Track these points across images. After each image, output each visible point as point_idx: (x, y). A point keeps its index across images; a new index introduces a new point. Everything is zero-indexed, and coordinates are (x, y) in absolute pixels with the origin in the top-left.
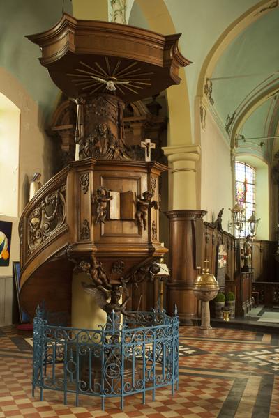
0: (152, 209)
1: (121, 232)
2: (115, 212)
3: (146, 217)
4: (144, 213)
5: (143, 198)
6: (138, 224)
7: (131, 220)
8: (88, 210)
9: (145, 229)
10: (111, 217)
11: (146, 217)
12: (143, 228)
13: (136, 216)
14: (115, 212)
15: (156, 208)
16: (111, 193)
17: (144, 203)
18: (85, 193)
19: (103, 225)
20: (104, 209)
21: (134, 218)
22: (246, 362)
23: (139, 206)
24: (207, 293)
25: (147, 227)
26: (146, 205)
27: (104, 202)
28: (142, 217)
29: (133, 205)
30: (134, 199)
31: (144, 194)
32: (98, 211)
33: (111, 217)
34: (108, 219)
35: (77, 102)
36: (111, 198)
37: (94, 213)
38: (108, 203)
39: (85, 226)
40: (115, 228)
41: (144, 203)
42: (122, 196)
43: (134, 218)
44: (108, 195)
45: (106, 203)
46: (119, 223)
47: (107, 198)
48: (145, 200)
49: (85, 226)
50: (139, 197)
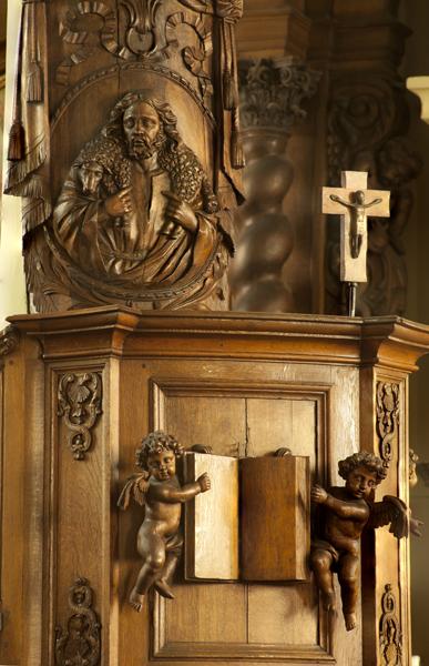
2: (214, 549)
5: (339, 482)
6: (318, 600)
7: (286, 583)
9: (349, 626)
13: (311, 564)
14: (214, 549)
15: (398, 531)
18: (83, 458)
19: (161, 606)
20: (167, 535)
21: (300, 574)
23: (322, 521)
27: (171, 501)
28: (339, 567)
30: (301, 485)
31: (347, 467)
33: (201, 571)
34: (184, 574)
38: (188, 508)
39: (80, 609)
40: (212, 620)
46: (233, 595)
48: (347, 494)
49: (80, 609)
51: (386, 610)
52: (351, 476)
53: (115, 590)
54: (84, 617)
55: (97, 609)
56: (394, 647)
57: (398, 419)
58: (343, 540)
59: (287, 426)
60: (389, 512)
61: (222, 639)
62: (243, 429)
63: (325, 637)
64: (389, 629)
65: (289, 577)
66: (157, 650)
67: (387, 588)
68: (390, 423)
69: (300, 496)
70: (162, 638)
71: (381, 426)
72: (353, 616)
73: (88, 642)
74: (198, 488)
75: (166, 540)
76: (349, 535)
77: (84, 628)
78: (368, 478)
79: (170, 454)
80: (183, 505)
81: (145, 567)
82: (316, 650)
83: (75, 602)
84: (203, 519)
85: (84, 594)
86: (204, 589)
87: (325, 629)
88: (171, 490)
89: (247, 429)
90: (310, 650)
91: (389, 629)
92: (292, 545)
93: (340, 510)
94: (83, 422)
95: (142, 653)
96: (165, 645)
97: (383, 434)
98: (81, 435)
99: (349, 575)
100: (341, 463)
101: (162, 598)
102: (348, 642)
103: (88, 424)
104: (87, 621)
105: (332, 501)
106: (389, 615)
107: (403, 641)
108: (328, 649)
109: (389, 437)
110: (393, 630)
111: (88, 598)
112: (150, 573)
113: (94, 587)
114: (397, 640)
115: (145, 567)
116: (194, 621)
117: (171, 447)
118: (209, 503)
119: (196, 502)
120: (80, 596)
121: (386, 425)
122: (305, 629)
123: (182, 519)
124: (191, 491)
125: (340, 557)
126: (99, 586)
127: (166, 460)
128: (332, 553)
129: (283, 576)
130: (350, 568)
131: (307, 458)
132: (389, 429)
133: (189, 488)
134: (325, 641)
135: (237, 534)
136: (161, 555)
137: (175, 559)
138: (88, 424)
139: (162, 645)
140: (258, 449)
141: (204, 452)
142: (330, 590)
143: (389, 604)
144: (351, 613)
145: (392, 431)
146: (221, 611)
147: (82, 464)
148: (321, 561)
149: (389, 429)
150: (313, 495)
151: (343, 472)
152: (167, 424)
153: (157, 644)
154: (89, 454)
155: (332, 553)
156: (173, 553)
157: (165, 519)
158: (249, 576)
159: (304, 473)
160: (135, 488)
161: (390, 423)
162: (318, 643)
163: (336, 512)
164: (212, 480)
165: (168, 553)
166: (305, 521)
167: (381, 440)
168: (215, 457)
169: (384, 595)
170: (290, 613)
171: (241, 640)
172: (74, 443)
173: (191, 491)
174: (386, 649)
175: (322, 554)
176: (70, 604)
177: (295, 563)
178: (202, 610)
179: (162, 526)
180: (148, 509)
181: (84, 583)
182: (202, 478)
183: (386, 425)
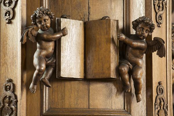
0: (155, 55)
1: (85, 106)
2: (71, 64)
3: (141, 74)
4: (136, 65)
5: (133, 32)
6: (123, 88)
7: (107, 80)
8: (13, 63)
9: (138, 100)
10: (65, 73)
11: (141, 74)
12: (135, 98)
13: (118, 71)
14: (71, 64)
15: (162, 54)
16: (65, 23)
17: (136, 44)
18: (10, 22)
19: (46, 91)
20: (47, 57)
21: (113, 75)
22: (168, 17)
23: (123, 50)
24: (47, 21)
25: (143, 95)
26: (139, 48)
27: (49, 40)
28: (131, 72)
29: (112, 48)
30: (114, 34)
31: (136, 24)
32: (36, 61)
33: (65, 73)
34: (56, 77)
35: (145, 39)
36: (64, 32)
37: (27, 65)
38: (58, 44)
39: (9, 93)
40: (73, 99)
41: (136, 44)
42: (88, 29)
43: (113, 75)
44: (56, 27)
45: (51, 45)
46: (82, 86)
47: (55, 32)
48: (137, 38)
49: (9, 93)
50: (125, 31)
51: (159, 93)
52: (138, 28)
53: (24, 84)
54: (10, 97)
55: (16, 93)
56: (163, 111)
57: (166, 4)
58: (134, 59)
59: (109, 7)
60: (157, 46)
61: (76, 107)
62: (87, 8)
63: (127, 106)
64: (160, 102)
65: (107, 76)
66: (44, 112)
67: (160, 83)
68: (161, 6)
69: (113, 39)
70: (47, 106)
71: (157, 8)
72: (140, 95)
73: (12, 109)
74: (62, 34)
75: (47, 59)
76: (137, 57)
77: (10, 102)
78: (146, 28)
79: (47, 17)
80: (55, 42)
81: (36, 72)
82: (123, 112)
83: (6, 89)
84: (65, 49)
85: (10, 86)
86: (68, 84)
87: (128, 102)
88: (47, 35)
89: (89, 8)
90: (120, 112)
91: (160, 102)
92: (109, 62)
93: (132, 44)
94: (10, 5)
95: (38, 114)
96: (49, 109)
97: (157, 11)
98: (9, 12)
99: (137, 75)
100: (133, 22)
101: (47, 88)
102: (139, 108)
103: (12, 6)
104: (12, 99)
105: (128, 40)
106: (160, 96)
107: (169, 108)
108: (129, 111)
109: (161, 12)
110: (162, 103)
111: (12, 88)
112: (38, 75)
113: (15, 82)
114: (165, 108)
115: (36, 72)
116: (63, 98)
117: (47, 14)
118: (68, 42)
119: (62, 41)
120: (8, 87)
121: (159, 7)
122: (117, 102)
123: (55, 49)
124: (58, 35)
125: (133, 68)
126: (17, 82)
127: (45, 20)
128: (129, 65)
129: (104, 76)
130: (137, 72)
131: (117, 21)
132: (161, 9)
133: (57, 34)
134: (127, 108)
135: (83, 57)
136: (43, 66)
137: (52, 69)
138: (12, 6)
139: (47, 109)
140: (95, 16)
141: (66, 18)
142: (128, 83)
143: (160, 91)
144: (139, 94)
145: (163, 10)
146: (76, 93)
147: (10, 25)
148: (123, 69)
149: (161, 9)
150: (118, 38)
151: (135, 28)
152: (50, 5)
153: (45, 109)
154: (13, 21)
155: (129, 65)
156: (51, 66)
157: (45, 49)
158: (89, 77)
159: (115, 28)
160: (29, 33)
161: (161, 6)
162: (124, 109)
163: (131, 46)
164: (68, 30)
165: (47, 66)
166: (116, 51)
167: (156, 13)
168: (71, 20)
169: (158, 87)
170: (109, 95)
171: (85, 107)
172: (6, 15)
173: (58, 35)
174: (158, 111)
175: (124, 66)
176: (4, 91)
177: (110, 70)
178: (67, 93)
179: (44, 53)
180: (38, 45)
181: (10, 81)
182: (64, 29)
183: (159, 7)
